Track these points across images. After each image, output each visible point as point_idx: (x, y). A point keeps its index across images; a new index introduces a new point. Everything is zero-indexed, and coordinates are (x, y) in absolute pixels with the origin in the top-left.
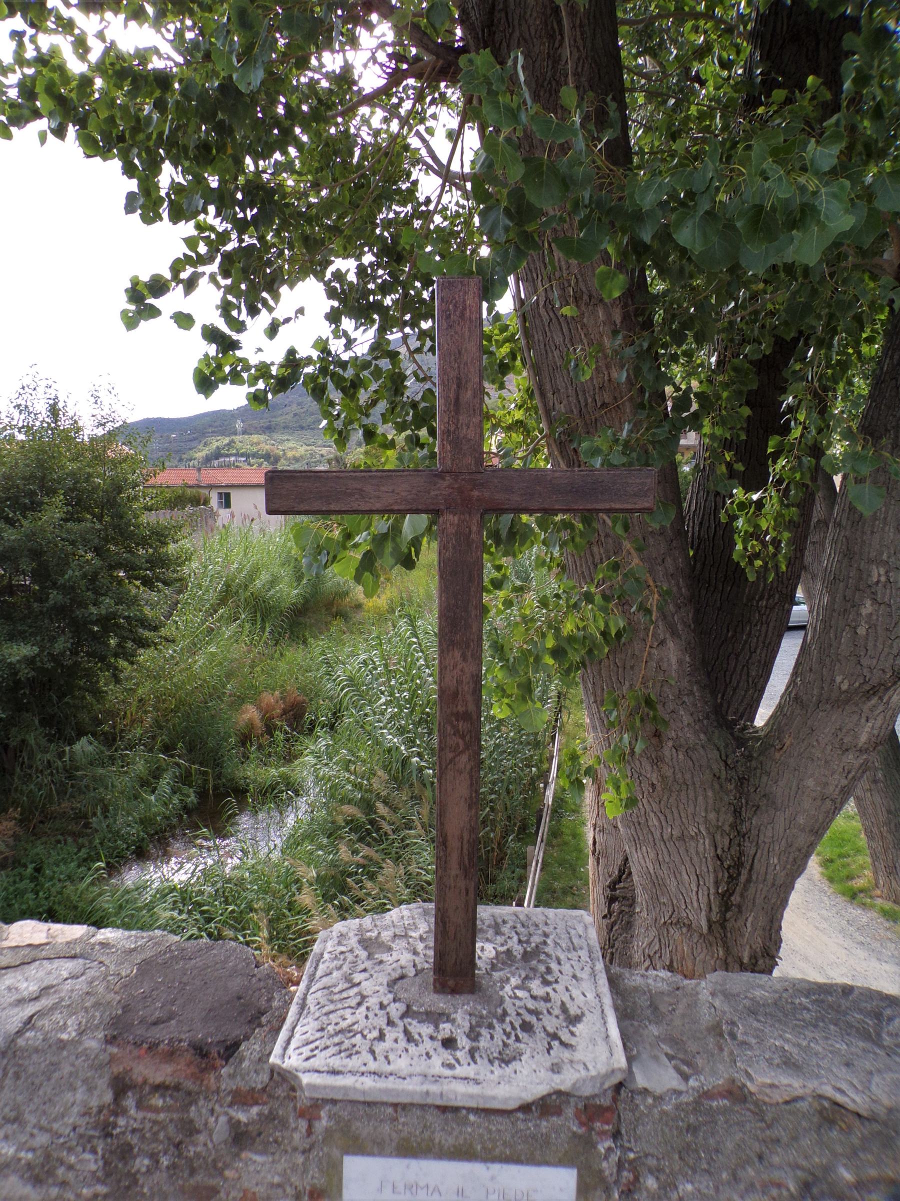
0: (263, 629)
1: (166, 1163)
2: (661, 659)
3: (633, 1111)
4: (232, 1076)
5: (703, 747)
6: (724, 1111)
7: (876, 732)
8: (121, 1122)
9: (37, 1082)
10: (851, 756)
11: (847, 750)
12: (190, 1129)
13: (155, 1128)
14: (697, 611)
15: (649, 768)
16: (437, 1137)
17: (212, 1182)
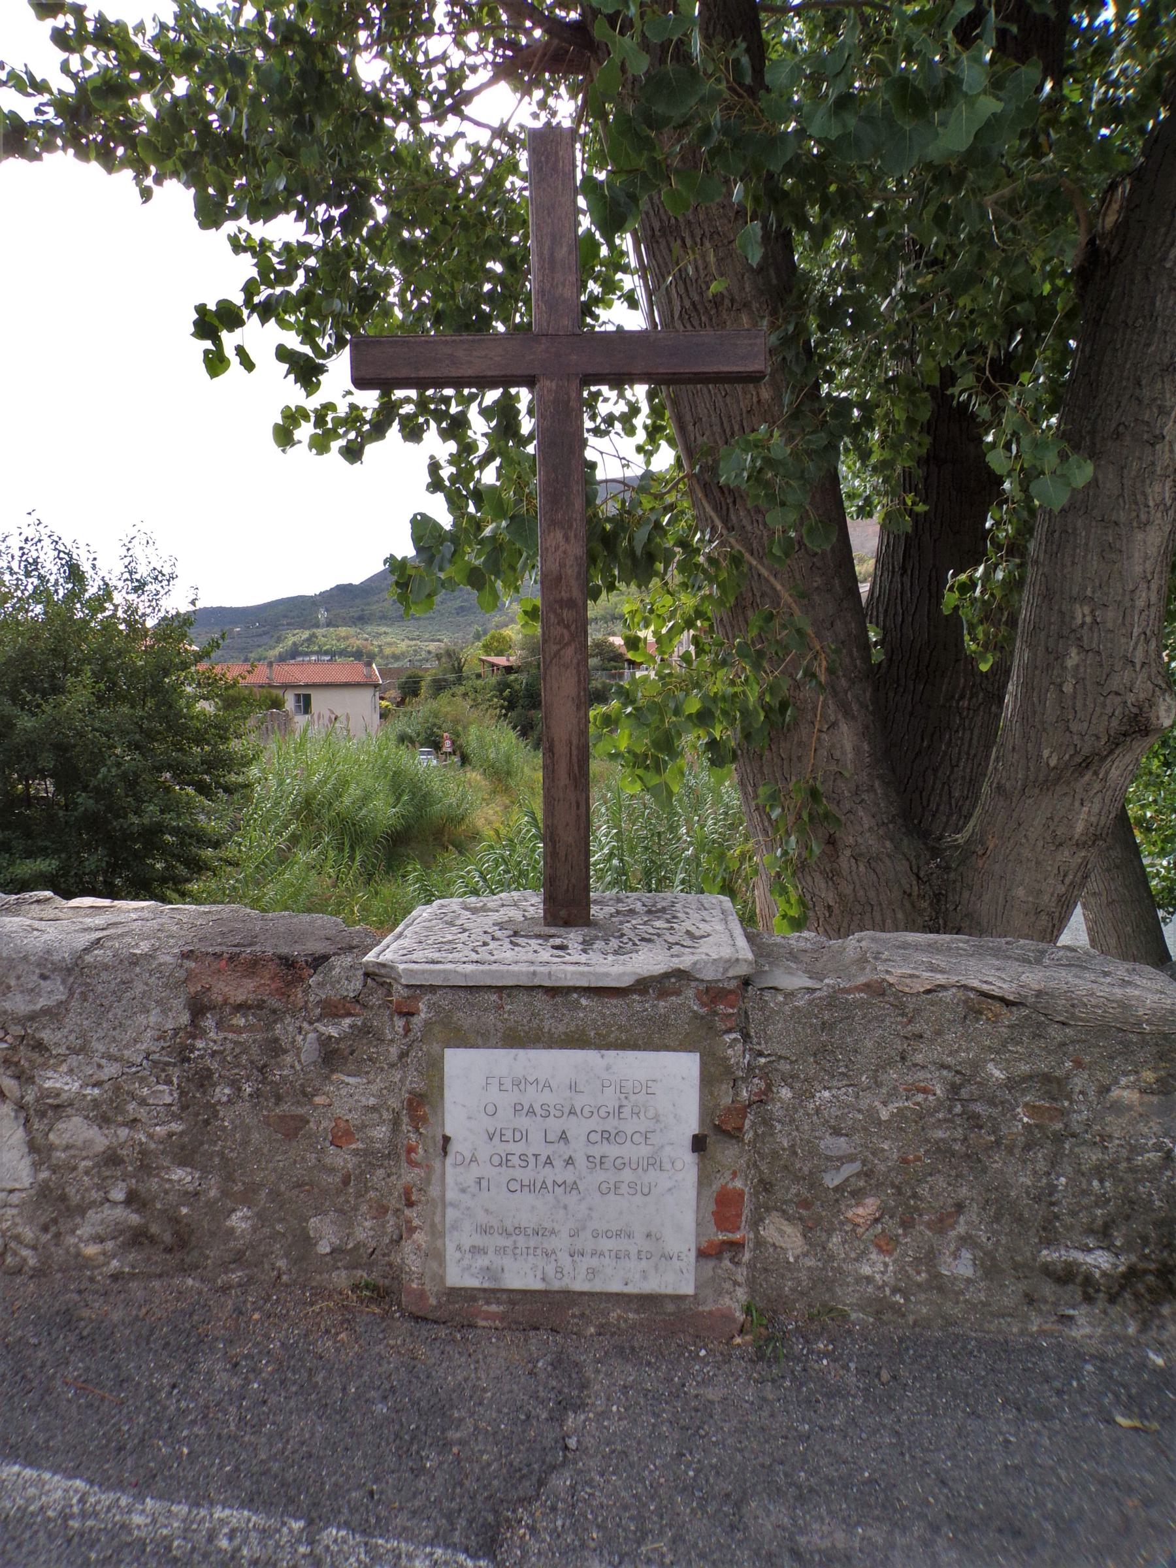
0: (352, 858)
1: (249, 1090)
2: (833, 746)
3: (762, 1009)
4: (321, 985)
5: (889, 856)
6: (862, 1004)
7: (1093, 819)
8: (200, 1044)
9: (106, 1003)
10: (1066, 853)
11: (1061, 845)
12: (275, 1048)
13: (237, 1050)
14: (876, 690)
15: (823, 885)
16: (547, 1025)
17: (301, 1111)
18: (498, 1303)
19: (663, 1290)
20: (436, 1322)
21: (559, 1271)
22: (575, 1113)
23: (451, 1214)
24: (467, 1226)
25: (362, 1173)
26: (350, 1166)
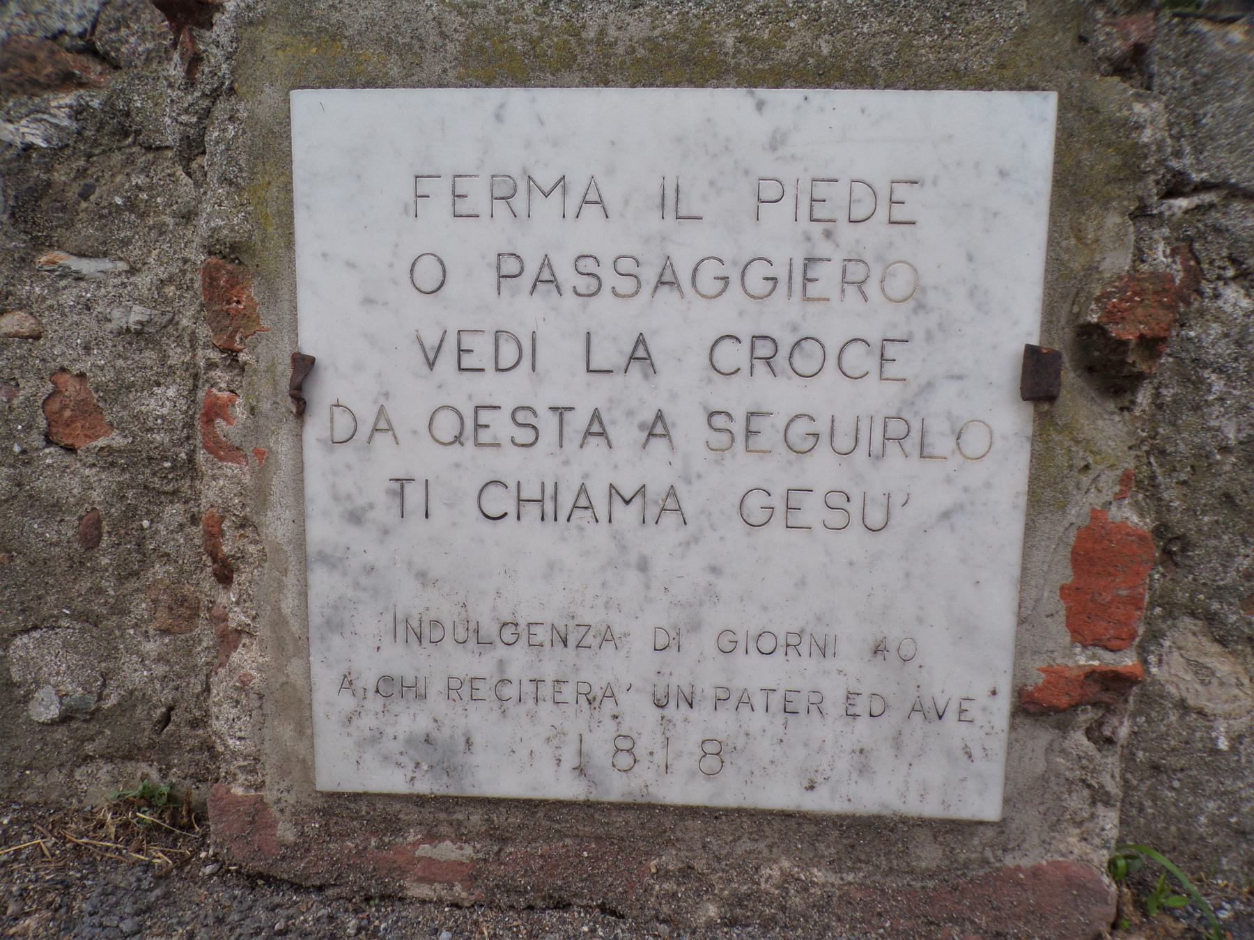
18: (461, 837)
19: (915, 807)
20: (297, 887)
21: (625, 746)
22: (674, 284)
23: (322, 584)
24: (369, 623)
25: (131, 514)
26: (96, 496)
